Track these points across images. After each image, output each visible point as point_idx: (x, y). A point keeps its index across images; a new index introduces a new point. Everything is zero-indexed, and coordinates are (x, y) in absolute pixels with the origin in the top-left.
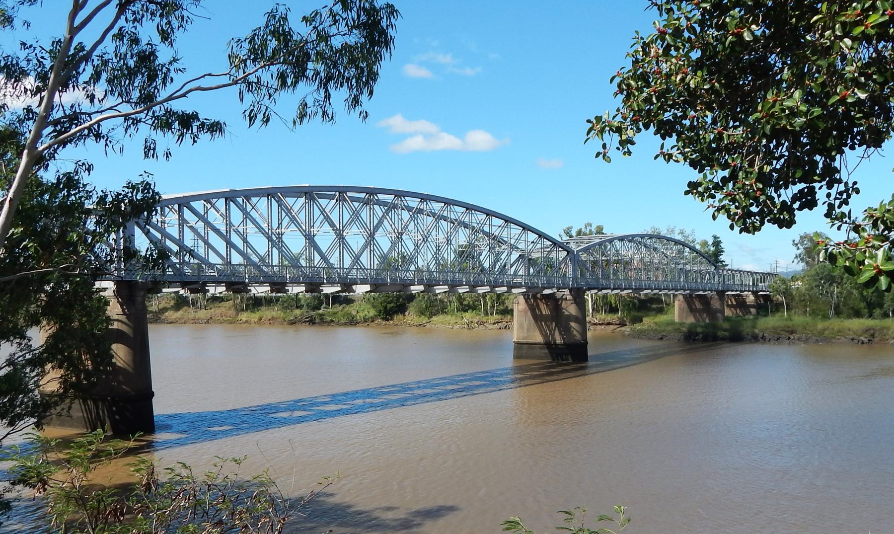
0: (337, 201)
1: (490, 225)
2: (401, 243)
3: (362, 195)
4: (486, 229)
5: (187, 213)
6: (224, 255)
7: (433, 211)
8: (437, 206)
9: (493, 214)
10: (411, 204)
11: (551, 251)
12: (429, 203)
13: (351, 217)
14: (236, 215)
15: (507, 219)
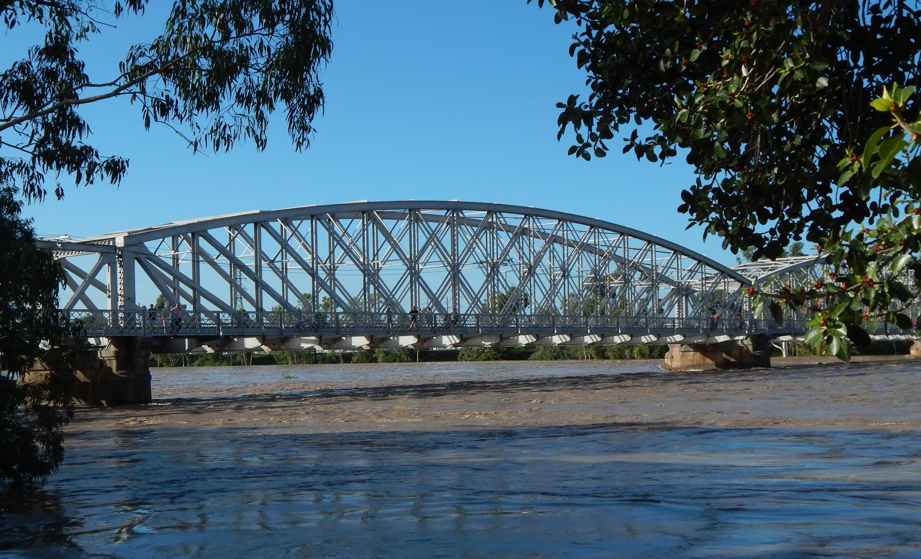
0: (448, 224)
1: (627, 249)
2: (534, 278)
3: (442, 213)
4: (620, 252)
5: (202, 242)
6: (254, 297)
7: (542, 231)
8: (549, 225)
9: (629, 232)
10: (510, 222)
11: (717, 283)
12: (536, 220)
13: (467, 246)
14: (270, 247)
15: (650, 239)
